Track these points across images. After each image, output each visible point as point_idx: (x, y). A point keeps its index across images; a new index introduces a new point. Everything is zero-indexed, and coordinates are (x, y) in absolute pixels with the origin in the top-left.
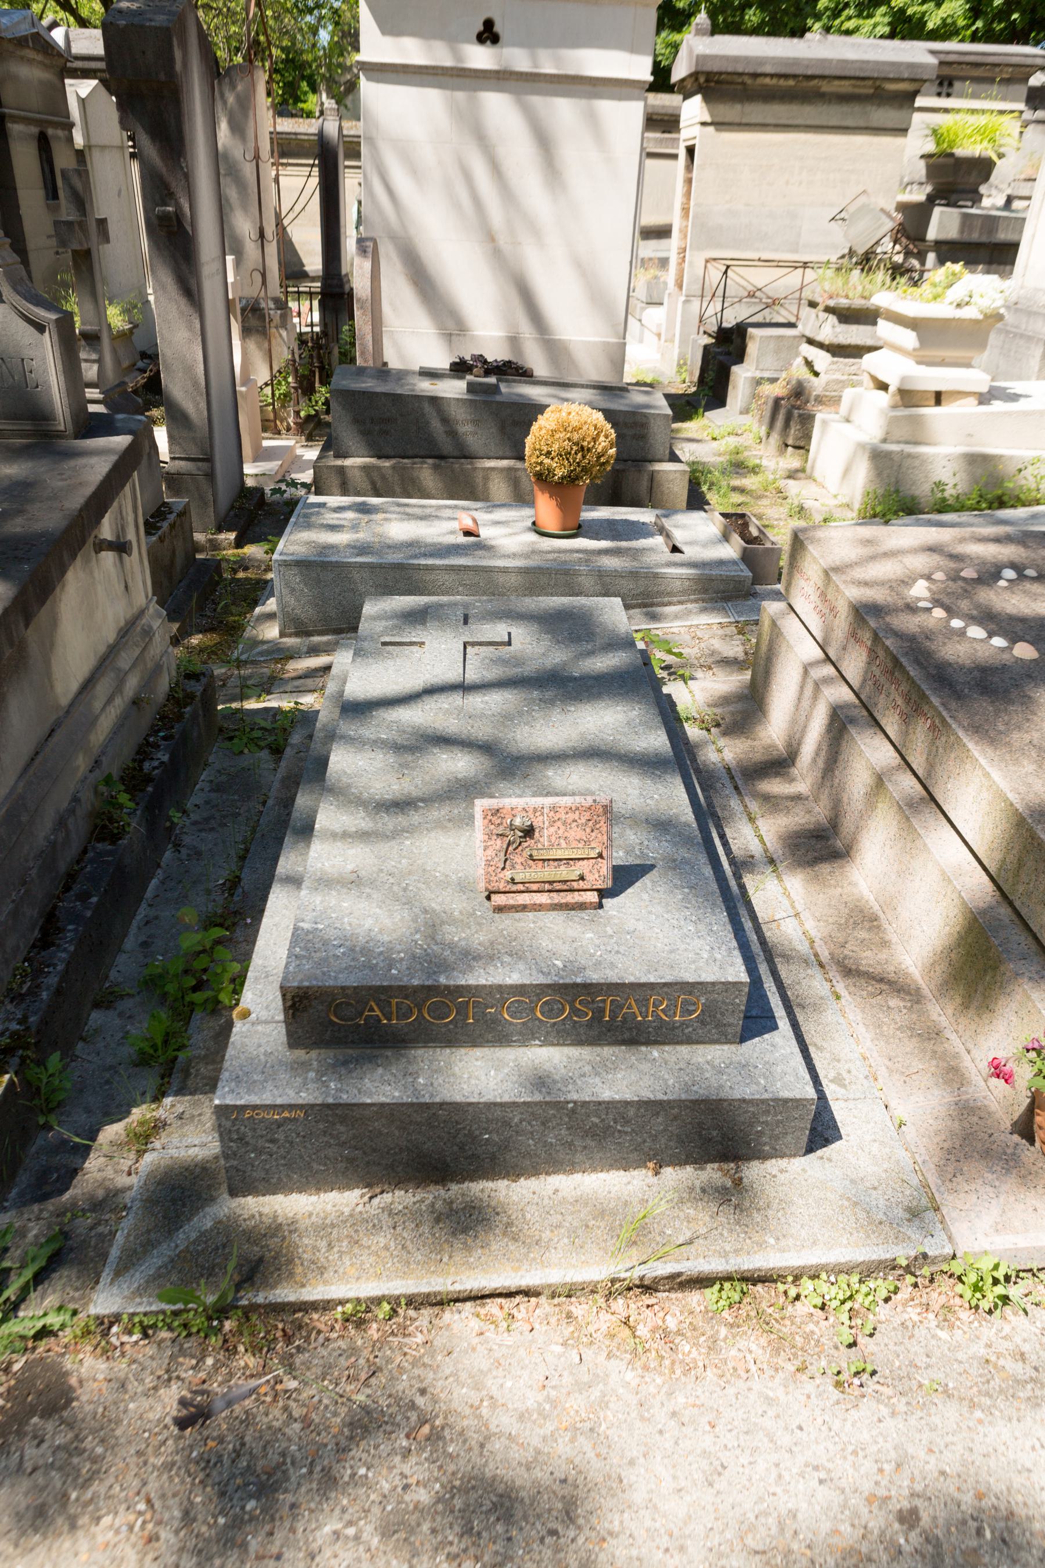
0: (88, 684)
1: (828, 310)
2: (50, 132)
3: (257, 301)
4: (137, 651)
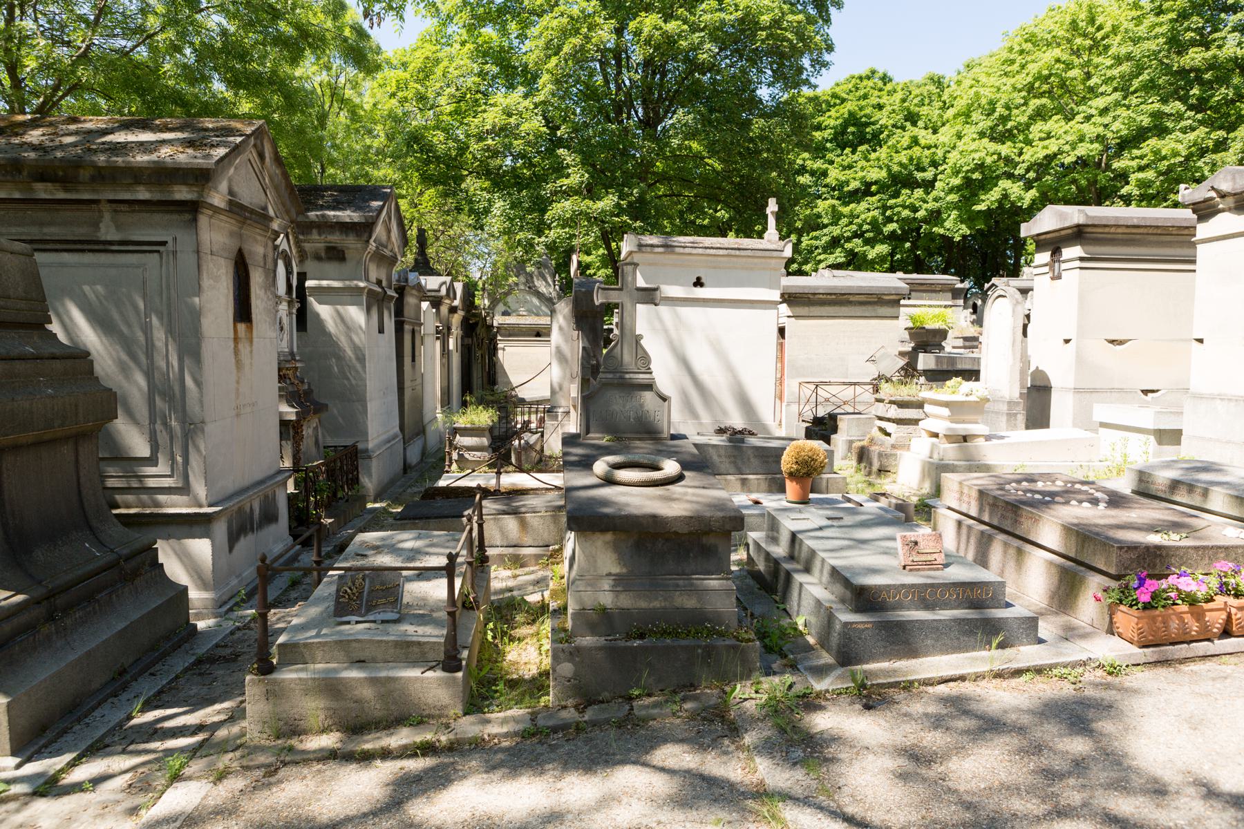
1: (891, 402)
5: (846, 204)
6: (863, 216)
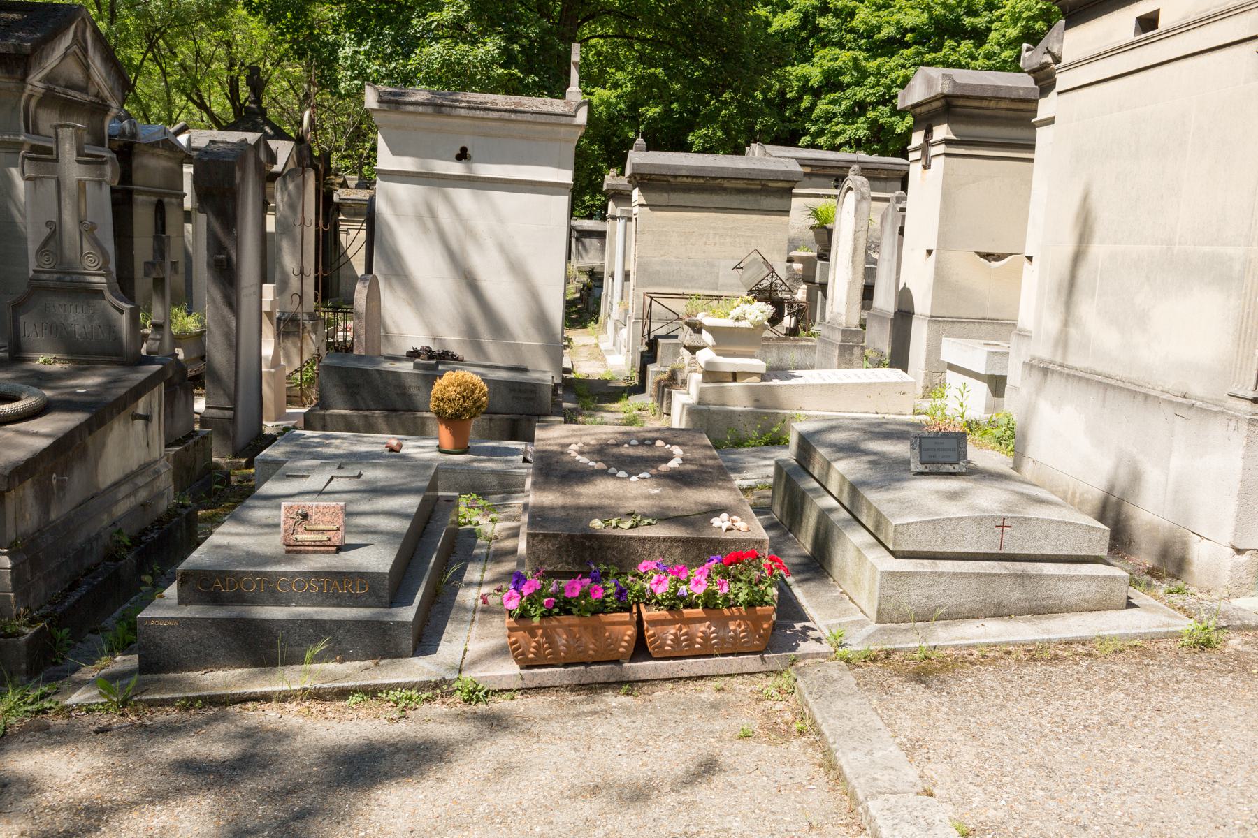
0: (117, 484)
2: (166, 200)
3: (295, 314)
4: (149, 479)
5: (874, 57)
6: (893, 76)
